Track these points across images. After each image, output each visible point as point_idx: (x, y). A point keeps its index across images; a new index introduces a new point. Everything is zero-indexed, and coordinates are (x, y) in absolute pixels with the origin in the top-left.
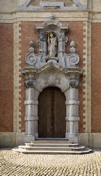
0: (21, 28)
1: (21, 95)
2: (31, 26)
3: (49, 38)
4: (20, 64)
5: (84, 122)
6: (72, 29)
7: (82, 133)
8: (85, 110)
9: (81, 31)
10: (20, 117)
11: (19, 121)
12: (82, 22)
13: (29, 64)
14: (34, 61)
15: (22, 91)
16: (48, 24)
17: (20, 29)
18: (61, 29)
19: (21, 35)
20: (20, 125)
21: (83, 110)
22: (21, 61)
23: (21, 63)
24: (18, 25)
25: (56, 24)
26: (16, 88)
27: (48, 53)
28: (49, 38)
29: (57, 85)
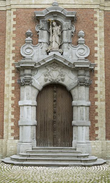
0: (15, 15)
1: (15, 95)
2: (29, 14)
3: (51, 26)
4: (13, 57)
5: (96, 128)
6: (80, 17)
7: (94, 140)
8: (97, 113)
9: (91, 19)
10: (12, 121)
11: (12, 126)
12: (92, 10)
13: (25, 57)
14: (31, 53)
15: (15, 89)
16: (50, 11)
17: (15, 16)
18: (67, 17)
19: (15, 23)
20: (13, 131)
21: (95, 113)
22: (14, 53)
23: (14, 56)
24: (12, 12)
25: (60, 12)
26: (8, 85)
27: (49, 43)
28: (51, 26)
29: (61, 82)
